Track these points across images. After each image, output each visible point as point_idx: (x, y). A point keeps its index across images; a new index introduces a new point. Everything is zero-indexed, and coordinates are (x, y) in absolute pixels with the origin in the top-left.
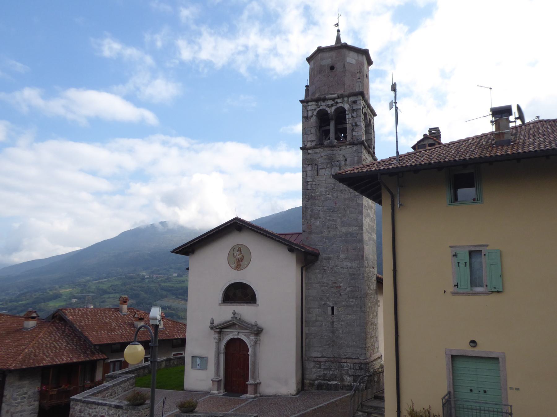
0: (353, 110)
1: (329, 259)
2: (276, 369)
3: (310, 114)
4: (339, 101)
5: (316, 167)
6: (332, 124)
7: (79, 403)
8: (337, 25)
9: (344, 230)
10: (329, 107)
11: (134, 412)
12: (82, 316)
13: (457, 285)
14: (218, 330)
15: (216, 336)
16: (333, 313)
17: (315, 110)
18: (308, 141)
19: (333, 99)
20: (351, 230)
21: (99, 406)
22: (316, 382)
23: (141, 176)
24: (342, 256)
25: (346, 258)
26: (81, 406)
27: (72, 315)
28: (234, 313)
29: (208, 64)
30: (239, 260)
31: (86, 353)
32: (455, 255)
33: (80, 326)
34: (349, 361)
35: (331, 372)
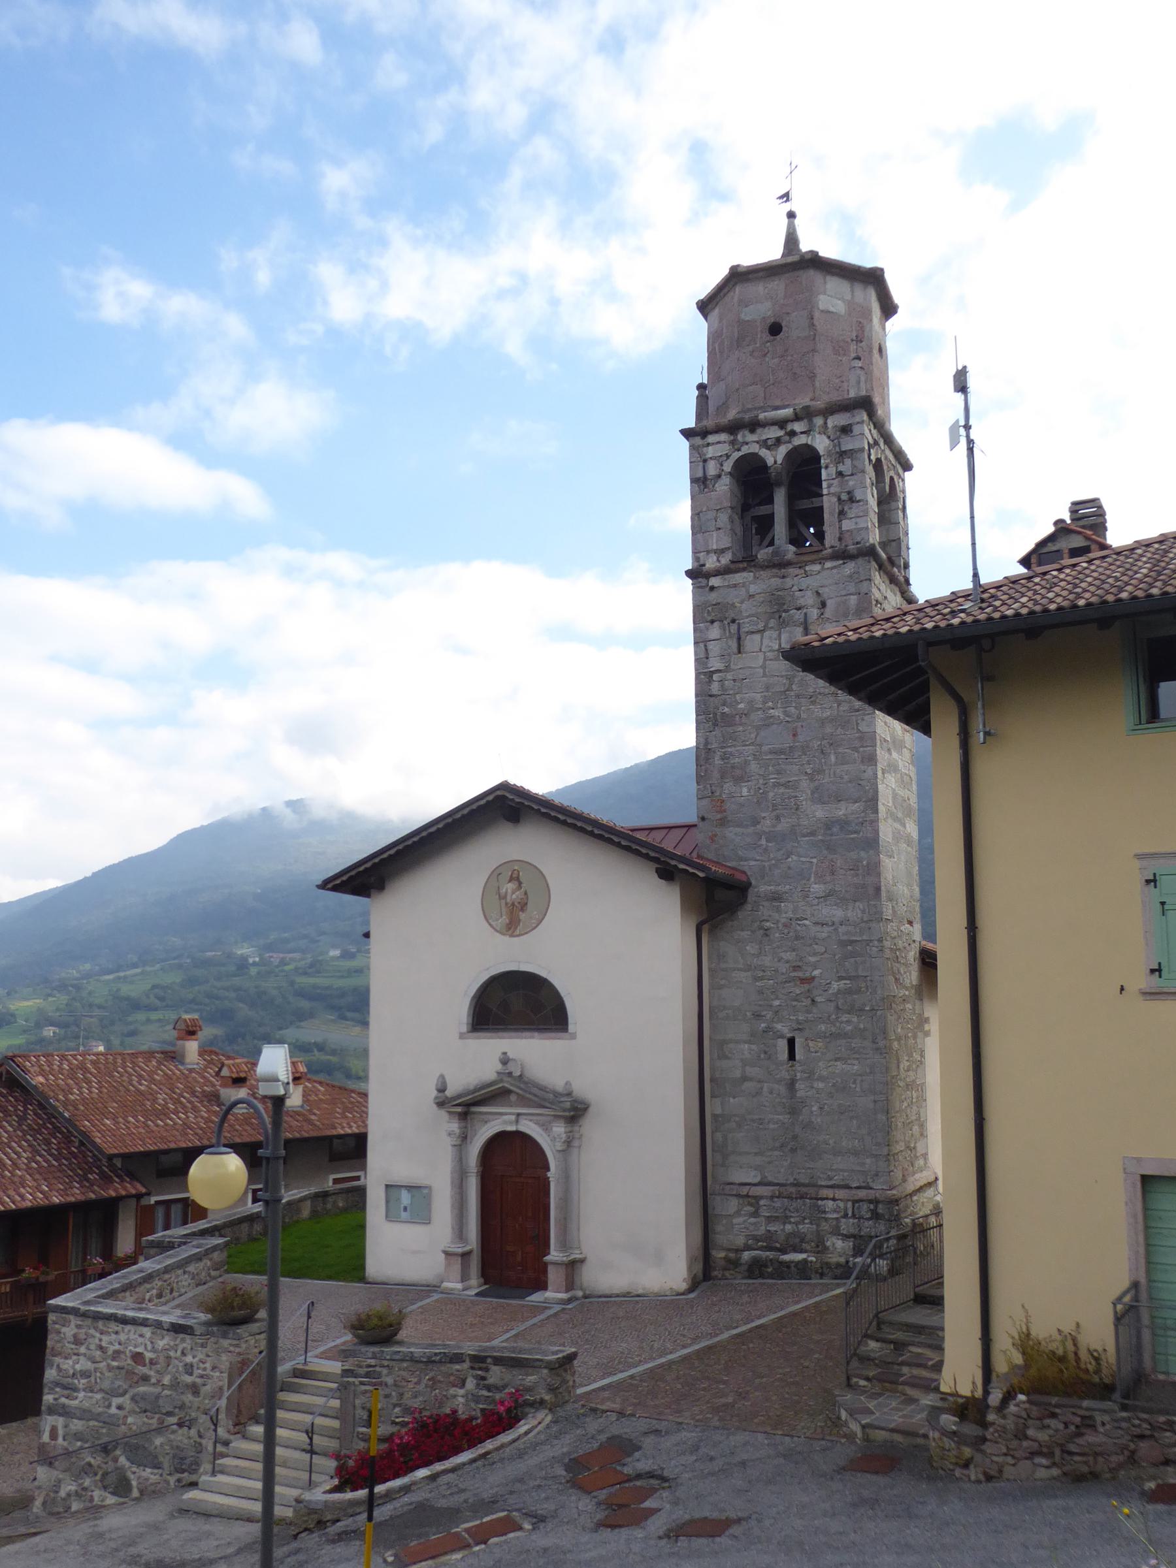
0: (842, 455)
1: (776, 898)
2: (630, 1220)
3: (712, 469)
4: (798, 427)
5: (734, 627)
7: (72, 1317)
8: (786, 197)
9: (820, 814)
10: (768, 448)
11: (225, 1343)
13: (1157, 971)
14: (459, 1109)
15: (455, 1126)
16: (792, 1056)
17: (728, 456)
18: (708, 552)
19: (782, 423)
20: (842, 810)
21: (128, 1327)
22: (746, 1256)
23: (226, 668)
24: (817, 888)
26: (78, 1327)
27: (42, 1073)
28: (505, 1060)
29: (412, 332)
30: (516, 906)
31: (88, 1180)
32: (1152, 881)
33: (66, 1104)
34: (840, 1193)
35: (788, 1227)
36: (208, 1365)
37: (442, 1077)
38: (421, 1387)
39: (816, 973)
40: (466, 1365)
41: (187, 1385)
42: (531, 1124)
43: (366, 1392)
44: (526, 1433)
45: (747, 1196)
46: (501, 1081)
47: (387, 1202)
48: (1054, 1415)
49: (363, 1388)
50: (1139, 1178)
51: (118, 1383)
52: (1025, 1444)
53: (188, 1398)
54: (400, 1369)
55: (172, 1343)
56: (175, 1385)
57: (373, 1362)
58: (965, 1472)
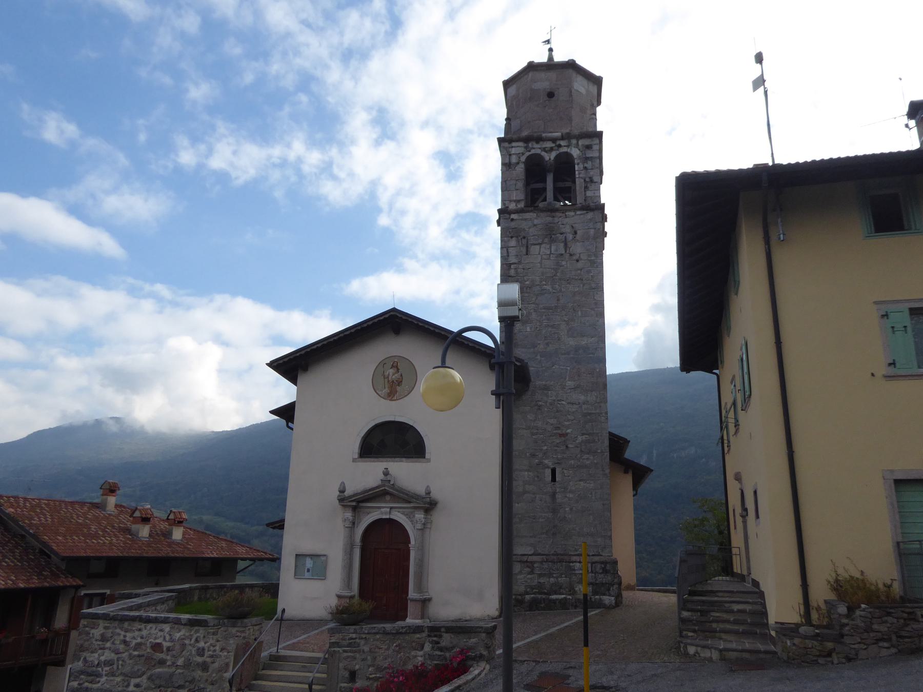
0: (587, 159)
1: (546, 388)
2: (460, 576)
3: (514, 159)
4: (563, 143)
5: (524, 241)
6: (550, 179)
7: (101, 622)
8: (548, 42)
10: (546, 152)
11: (234, 630)
12: (33, 508)
13: (893, 364)
14: (354, 504)
15: (349, 515)
16: (554, 479)
17: (523, 154)
18: (511, 201)
19: (554, 140)
20: (584, 342)
21: (150, 625)
22: (528, 597)
23: (82, 341)
24: (570, 384)
25: (575, 388)
26: (106, 628)
27: (12, 506)
28: (386, 473)
29: (222, 177)
30: (394, 383)
31: (43, 575)
32: (885, 316)
33: (31, 525)
36: (217, 648)
37: (343, 483)
38: (390, 651)
39: (569, 431)
40: (424, 635)
41: (198, 664)
42: (399, 515)
43: (348, 657)
44: (479, 674)
45: (527, 561)
46: (384, 486)
47: (296, 566)
48: (889, 614)
49: (345, 654)
50: (892, 481)
51: (136, 668)
52: (872, 635)
53: (198, 673)
54: (374, 640)
55: (187, 634)
56: (188, 665)
57: (354, 636)
58: (829, 659)
